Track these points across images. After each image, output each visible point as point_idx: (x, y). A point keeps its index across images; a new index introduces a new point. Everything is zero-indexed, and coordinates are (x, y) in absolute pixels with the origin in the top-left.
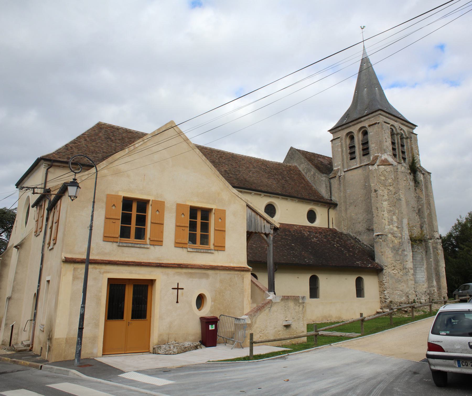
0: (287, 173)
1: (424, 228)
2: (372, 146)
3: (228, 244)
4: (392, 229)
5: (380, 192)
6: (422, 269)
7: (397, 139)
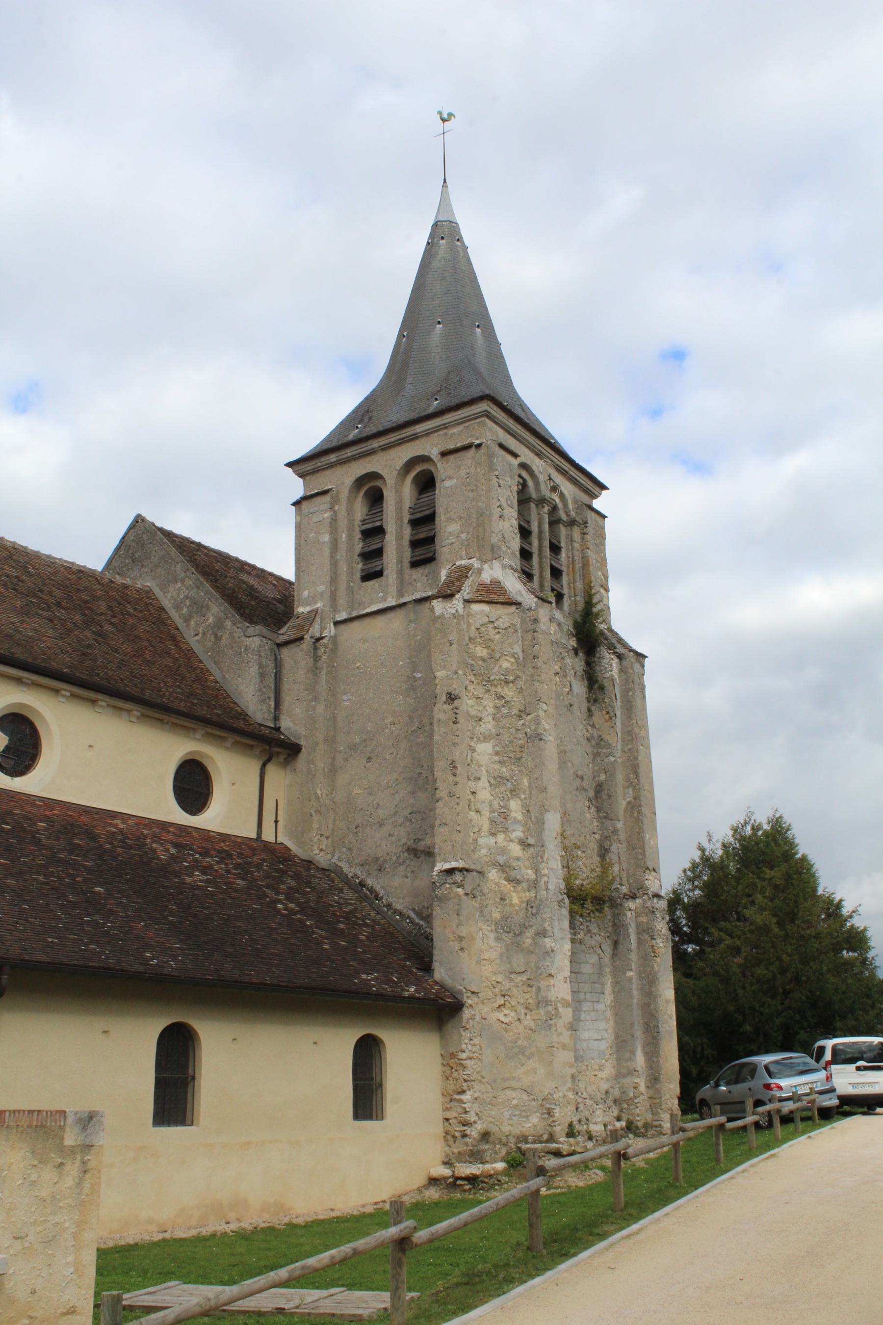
0: (110, 608)
1: (612, 857)
2: (449, 530)
4: (503, 851)
5: (467, 704)
6: (601, 1007)
7: (538, 520)
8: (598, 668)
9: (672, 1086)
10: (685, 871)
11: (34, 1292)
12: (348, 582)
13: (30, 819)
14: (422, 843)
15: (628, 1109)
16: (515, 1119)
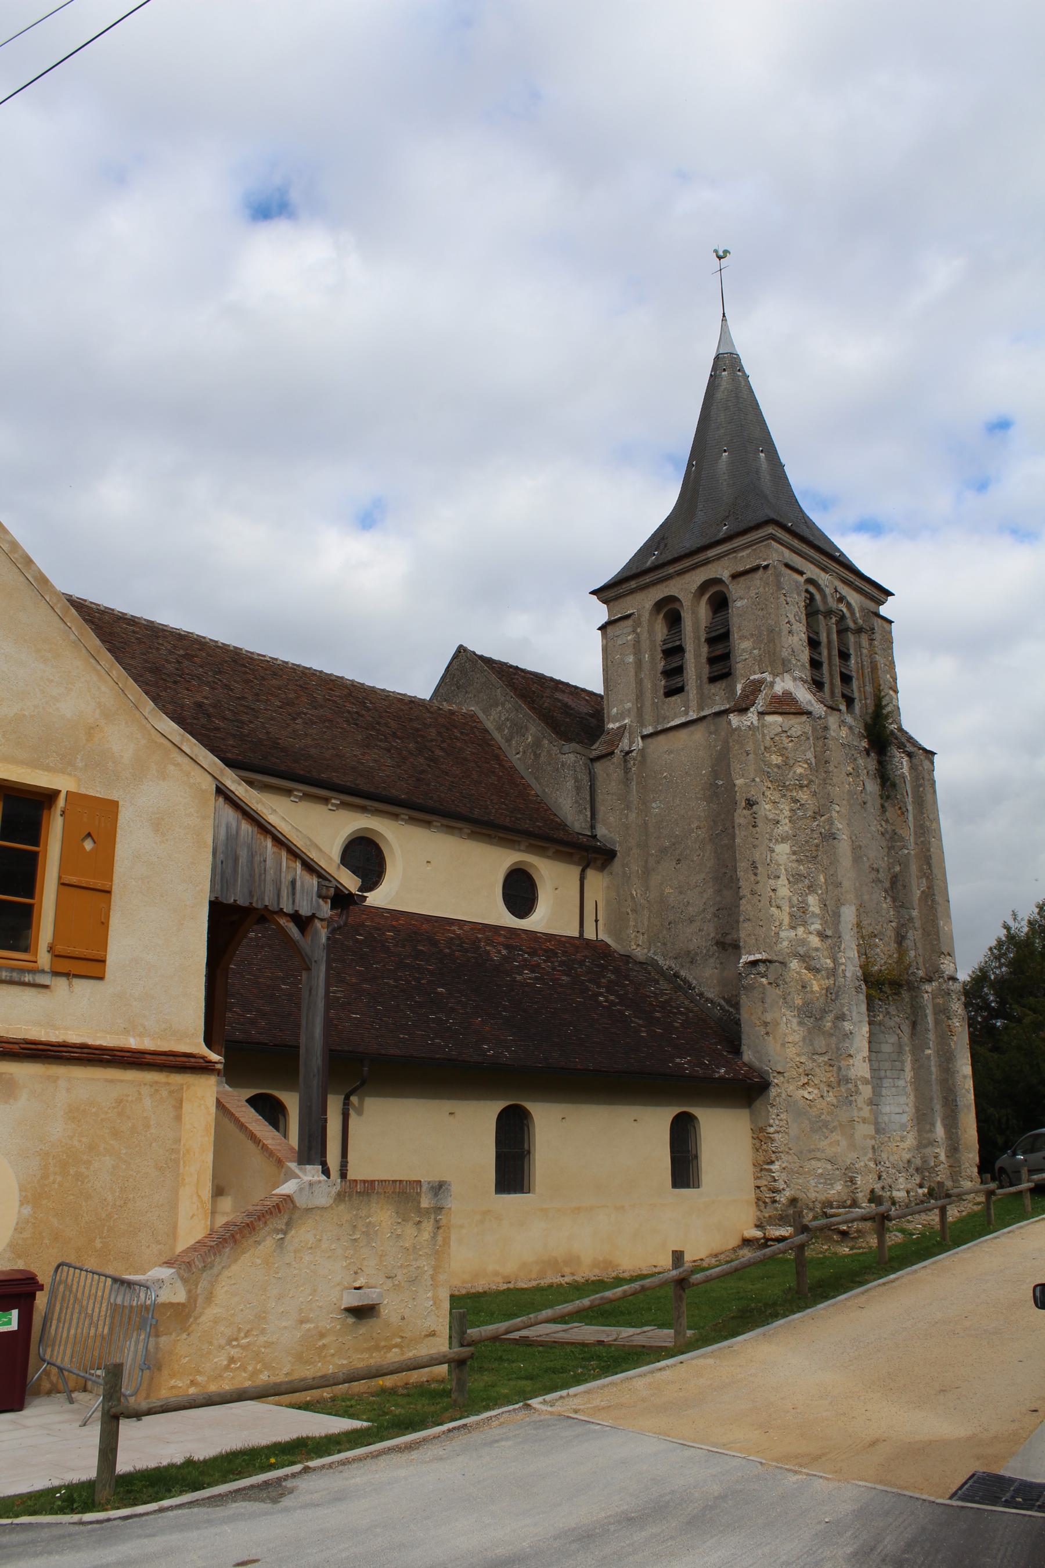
0: (439, 733)
1: (909, 943)
2: (743, 646)
3: (121, 946)
4: (803, 942)
5: (765, 808)
6: (901, 1083)
7: (827, 630)
8: (889, 767)
9: (971, 1156)
10: (991, 949)
11: (403, 1318)
12: (653, 698)
13: (379, 930)
14: (729, 937)
15: (929, 1177)
16: (821, 1186)
